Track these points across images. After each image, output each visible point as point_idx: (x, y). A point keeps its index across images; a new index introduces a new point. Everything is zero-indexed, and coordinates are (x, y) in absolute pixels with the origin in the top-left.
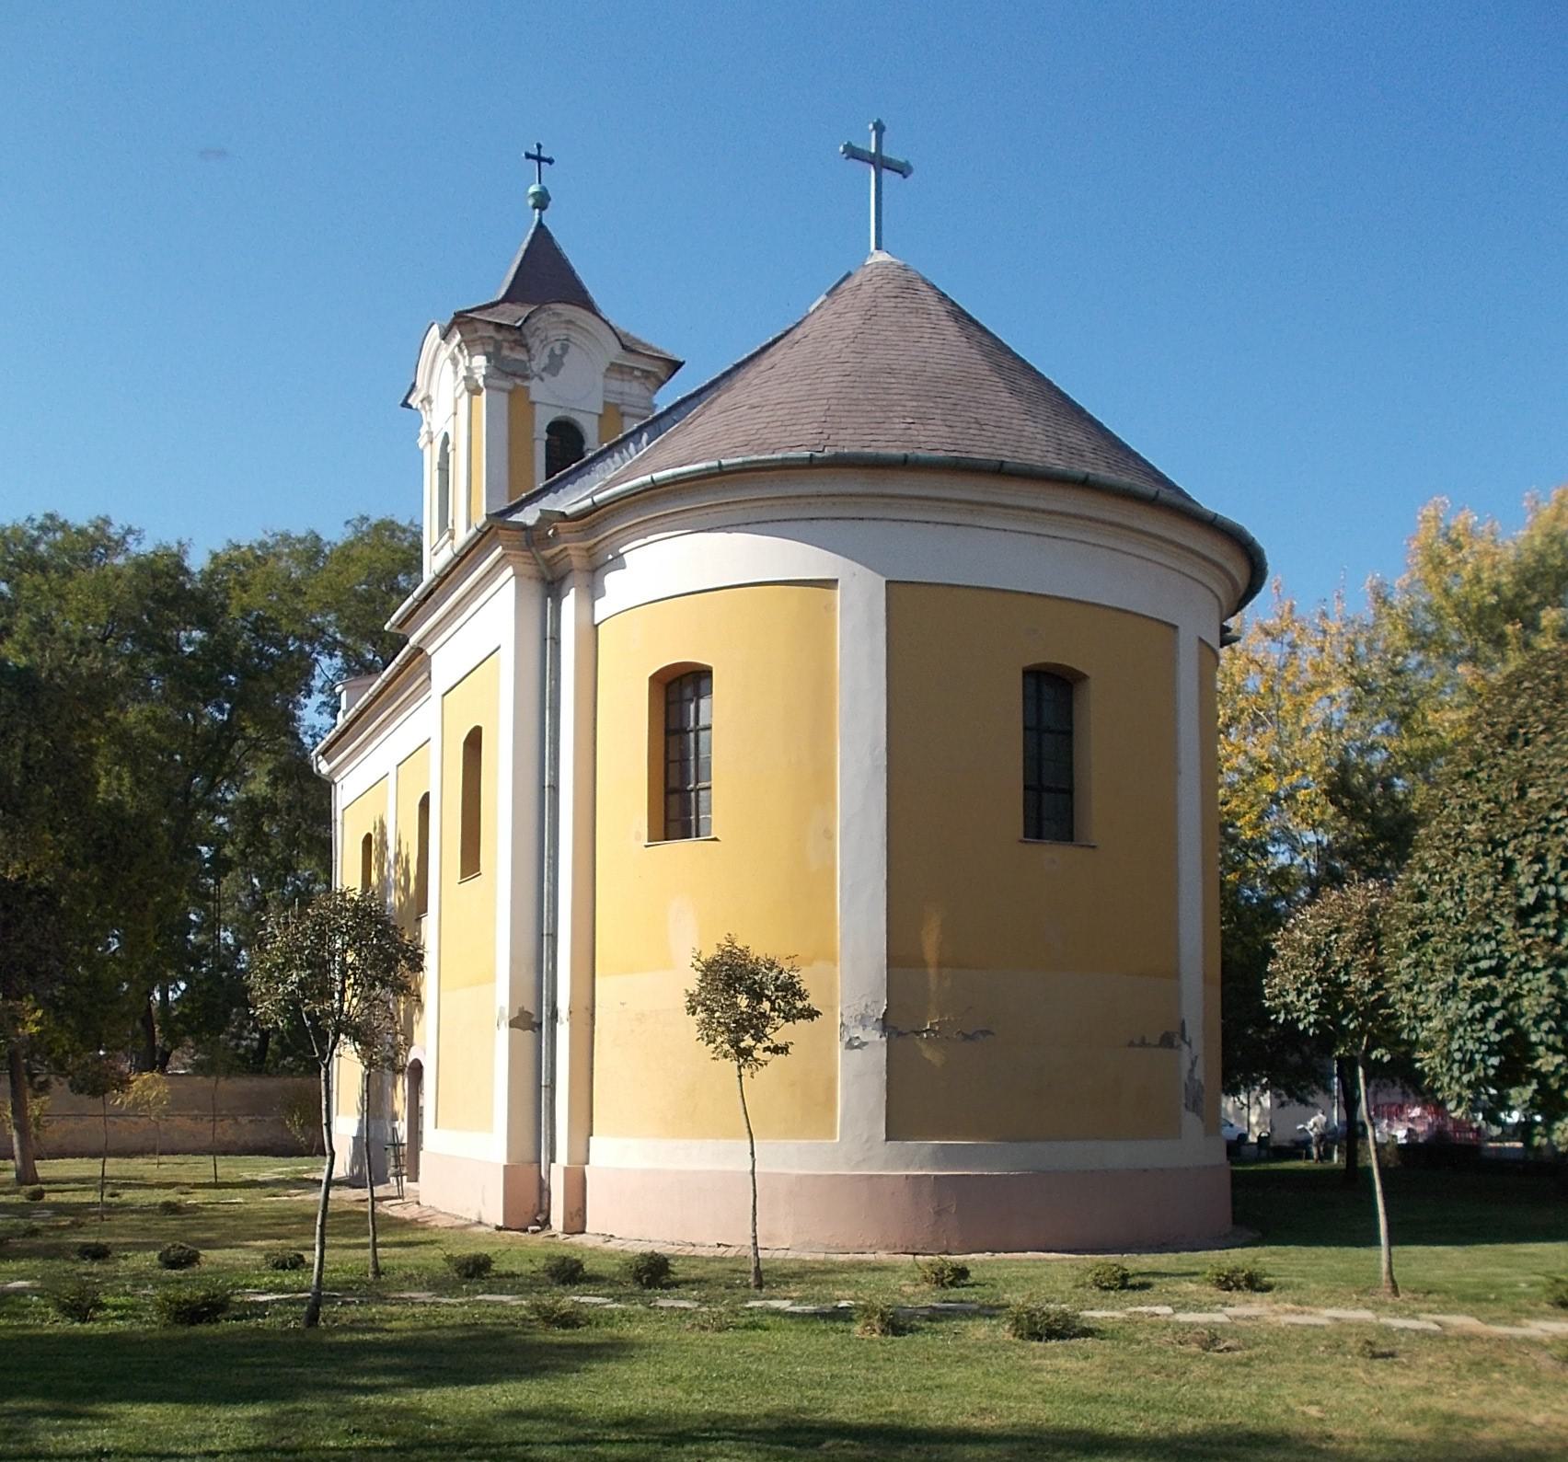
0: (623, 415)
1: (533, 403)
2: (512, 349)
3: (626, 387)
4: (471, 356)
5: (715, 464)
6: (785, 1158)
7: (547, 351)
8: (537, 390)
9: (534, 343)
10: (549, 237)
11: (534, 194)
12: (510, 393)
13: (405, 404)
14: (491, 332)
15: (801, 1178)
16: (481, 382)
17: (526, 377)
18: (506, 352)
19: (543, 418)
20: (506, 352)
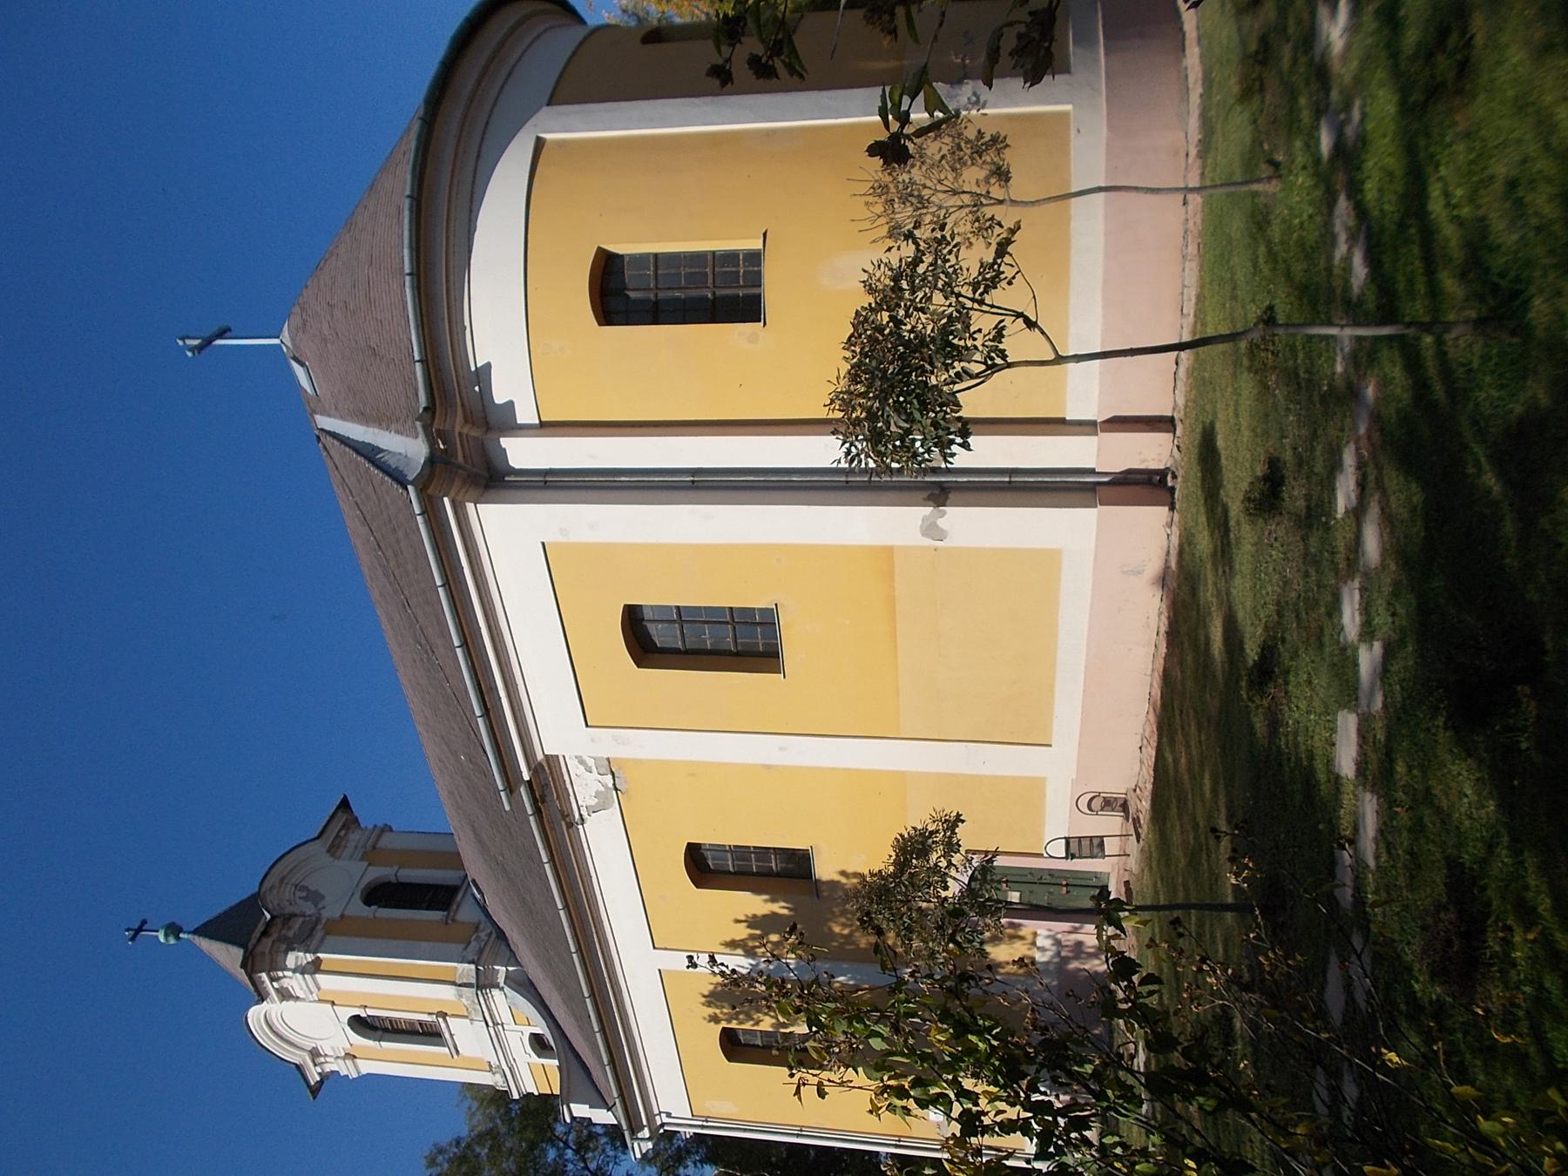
0: (374, 848)
1: (342, 916)
2: (289, 929)
3: (352, 844)
4: (285, 968)
5: (408, 278)
6: (1089, 159)
7: (301, 902)
8: (331, 911)
9: (289, 910)
10: (205, 925)
11: (166, 936)
12: (327, 933)
13: (315, 1091)
14: (267, 942)
15: (1110, 126)
16: (310, 957)
17: (318, 920)
18: (291, 934)
19: (358, 909)
20: (291, 934)
